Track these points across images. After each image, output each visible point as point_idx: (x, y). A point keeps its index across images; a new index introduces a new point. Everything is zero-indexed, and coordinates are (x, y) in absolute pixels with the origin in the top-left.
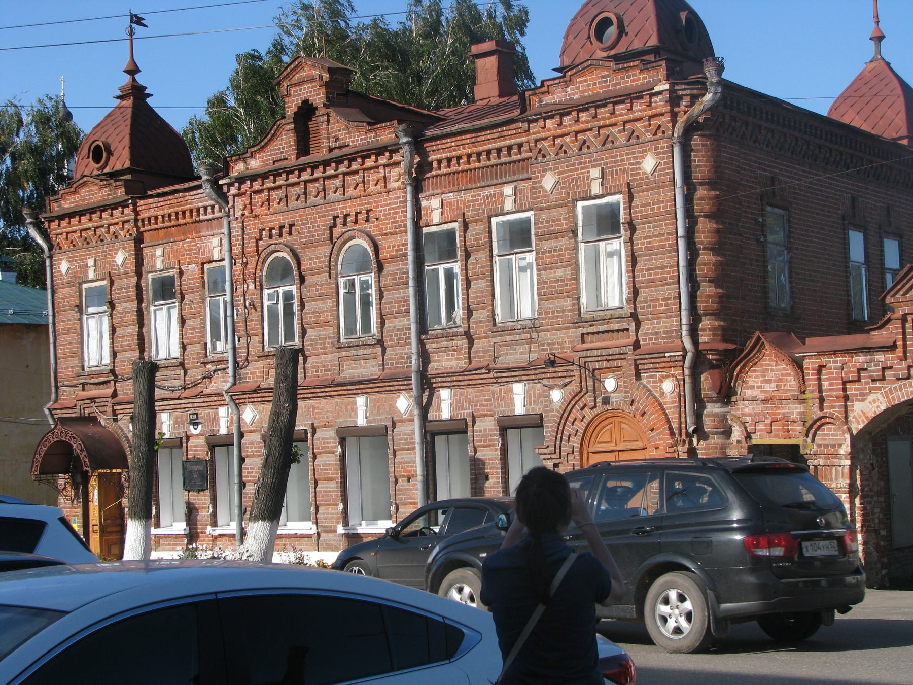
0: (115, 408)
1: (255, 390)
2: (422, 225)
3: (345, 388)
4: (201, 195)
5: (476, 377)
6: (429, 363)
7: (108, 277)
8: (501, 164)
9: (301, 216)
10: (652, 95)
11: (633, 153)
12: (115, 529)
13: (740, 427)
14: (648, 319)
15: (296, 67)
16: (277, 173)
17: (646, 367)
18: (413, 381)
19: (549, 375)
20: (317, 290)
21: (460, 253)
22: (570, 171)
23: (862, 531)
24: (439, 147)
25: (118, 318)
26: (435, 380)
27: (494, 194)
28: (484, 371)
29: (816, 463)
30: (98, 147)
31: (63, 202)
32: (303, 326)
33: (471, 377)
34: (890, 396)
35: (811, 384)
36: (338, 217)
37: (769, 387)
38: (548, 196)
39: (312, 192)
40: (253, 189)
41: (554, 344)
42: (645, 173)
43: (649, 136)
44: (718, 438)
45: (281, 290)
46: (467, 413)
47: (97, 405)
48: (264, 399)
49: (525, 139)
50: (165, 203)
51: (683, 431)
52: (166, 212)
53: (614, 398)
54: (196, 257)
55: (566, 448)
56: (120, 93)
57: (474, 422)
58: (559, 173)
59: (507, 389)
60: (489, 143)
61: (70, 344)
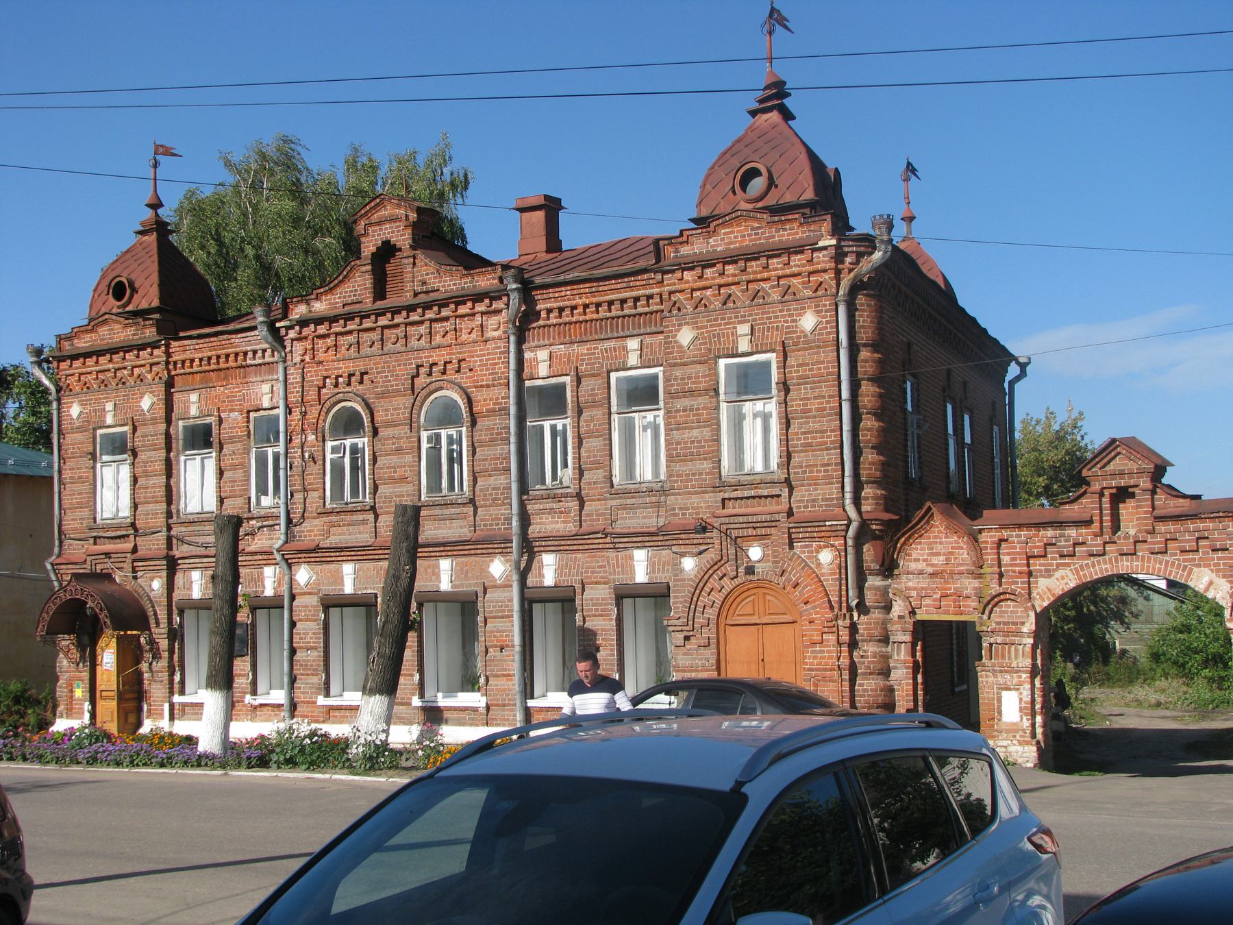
0: (135, 564)
1: (315, 550)
2: (524, 378)
3: (426, 549)
4: (251, 338)
5: (589, 542)
6: (529, 525)
7: (130, 423)
8: (624, 317)
9: (375, 364)
10: (814, 250)
11: (789, 310)
12: (132, 696)
13: (904, 602)
14: (803, 485)
15: (377, 205)
16: (349, 317)
17: (800, 536)
18: (514, 544)
19: (681, 542)
20: (393, 444)
21: (216, 445)
22: (711, 326)
23: (1042, 712)
24: (551, 295)
25: (141, 467)
26: (537, 544)
27: (615, 348)
28: (599, 535)
29: (992, 640)
30: (121, 283)
31: (76, 341)
32: (374, 481)
33: (582, 542)
34: (1081, 573)
35: (990, 558)
36: (423, 366)
37: (935, 560)
38: (684, 352)
39: (390, 338)
40: (317, 333)
41: (688, 509)
42: (802, 332)
43: (807, 293)
44: (879, 613)
45: (348, 442)
46: (576, 580)
47: (112, 560)
48: (323, 559)
49: (656, 290)
50: (205, 345)
51: (844, 605)
52: (205, 355)
53: (759, 568)
54: (241, 405)
55: (700, 620)
56: (141, 228)
57: (583, 590)
58: (698, 328)
59: (626, 556)
60: (612, 294)
61: (79, 494)
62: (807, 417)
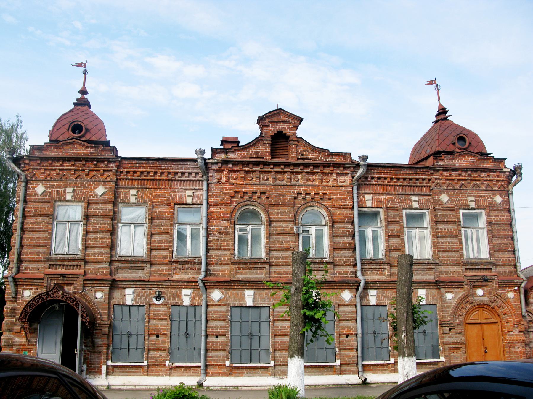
16: (257, 164)
42: (96, 195)
48: (152, 286)
62: (498, 238)
